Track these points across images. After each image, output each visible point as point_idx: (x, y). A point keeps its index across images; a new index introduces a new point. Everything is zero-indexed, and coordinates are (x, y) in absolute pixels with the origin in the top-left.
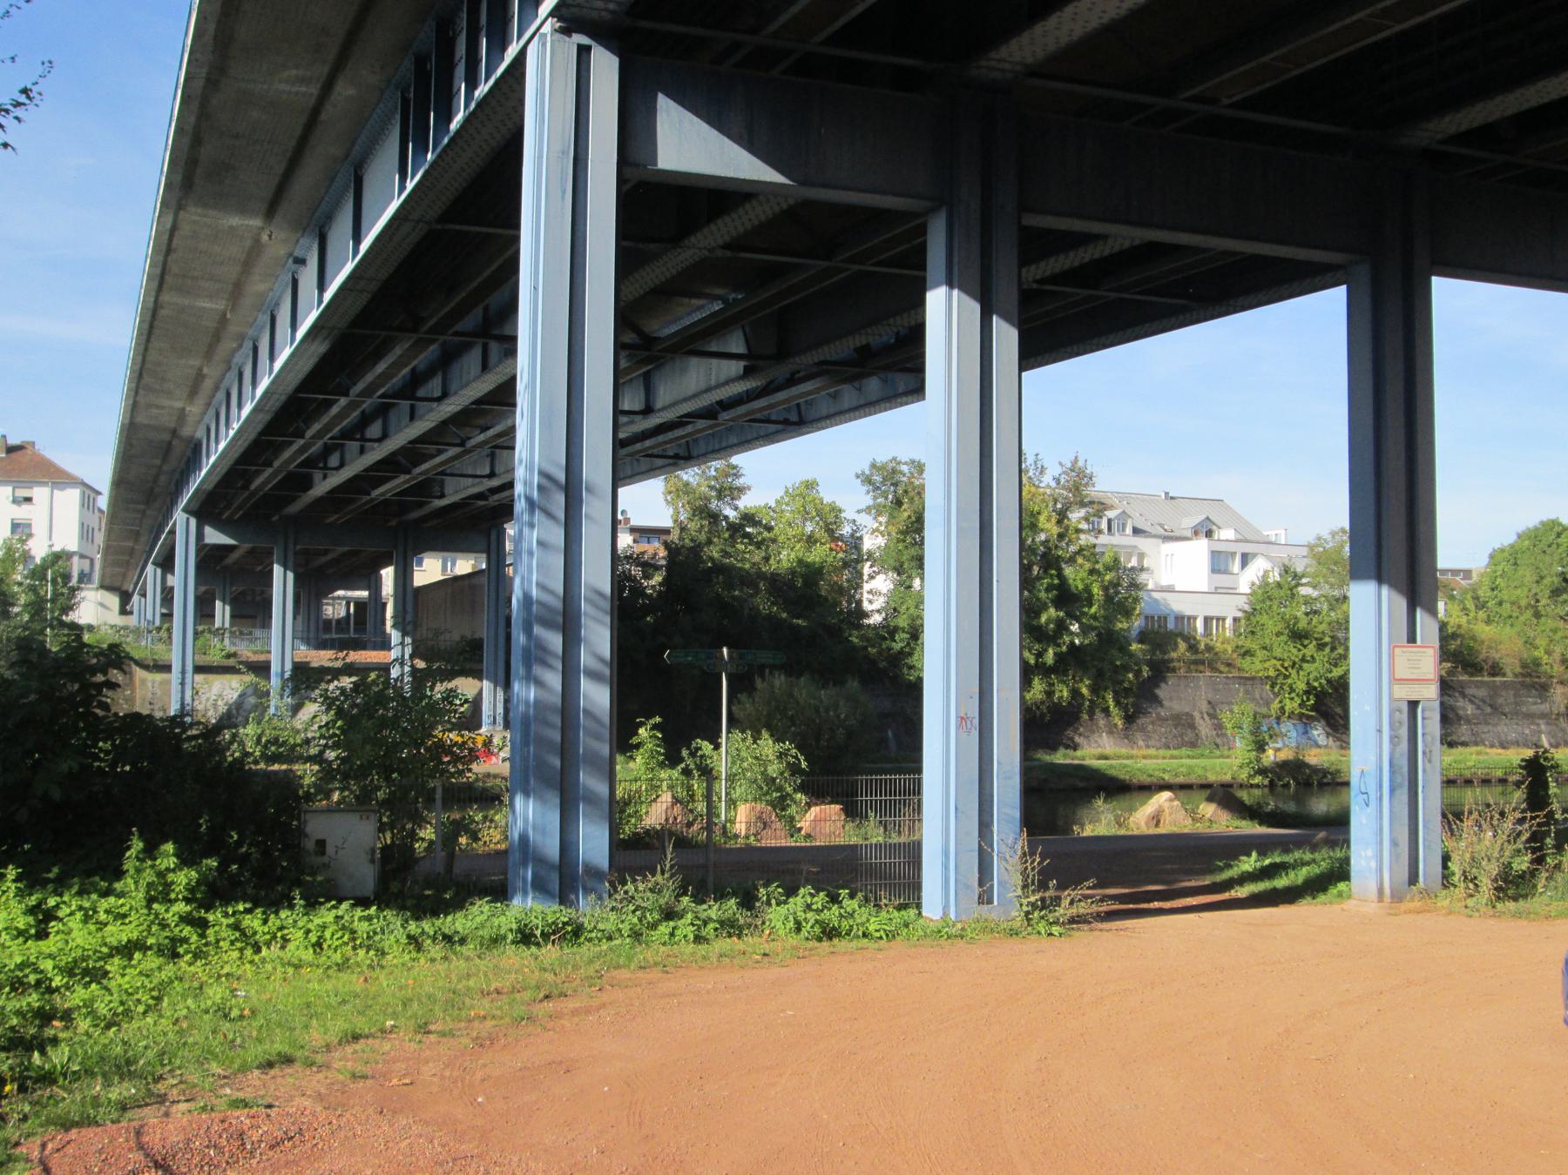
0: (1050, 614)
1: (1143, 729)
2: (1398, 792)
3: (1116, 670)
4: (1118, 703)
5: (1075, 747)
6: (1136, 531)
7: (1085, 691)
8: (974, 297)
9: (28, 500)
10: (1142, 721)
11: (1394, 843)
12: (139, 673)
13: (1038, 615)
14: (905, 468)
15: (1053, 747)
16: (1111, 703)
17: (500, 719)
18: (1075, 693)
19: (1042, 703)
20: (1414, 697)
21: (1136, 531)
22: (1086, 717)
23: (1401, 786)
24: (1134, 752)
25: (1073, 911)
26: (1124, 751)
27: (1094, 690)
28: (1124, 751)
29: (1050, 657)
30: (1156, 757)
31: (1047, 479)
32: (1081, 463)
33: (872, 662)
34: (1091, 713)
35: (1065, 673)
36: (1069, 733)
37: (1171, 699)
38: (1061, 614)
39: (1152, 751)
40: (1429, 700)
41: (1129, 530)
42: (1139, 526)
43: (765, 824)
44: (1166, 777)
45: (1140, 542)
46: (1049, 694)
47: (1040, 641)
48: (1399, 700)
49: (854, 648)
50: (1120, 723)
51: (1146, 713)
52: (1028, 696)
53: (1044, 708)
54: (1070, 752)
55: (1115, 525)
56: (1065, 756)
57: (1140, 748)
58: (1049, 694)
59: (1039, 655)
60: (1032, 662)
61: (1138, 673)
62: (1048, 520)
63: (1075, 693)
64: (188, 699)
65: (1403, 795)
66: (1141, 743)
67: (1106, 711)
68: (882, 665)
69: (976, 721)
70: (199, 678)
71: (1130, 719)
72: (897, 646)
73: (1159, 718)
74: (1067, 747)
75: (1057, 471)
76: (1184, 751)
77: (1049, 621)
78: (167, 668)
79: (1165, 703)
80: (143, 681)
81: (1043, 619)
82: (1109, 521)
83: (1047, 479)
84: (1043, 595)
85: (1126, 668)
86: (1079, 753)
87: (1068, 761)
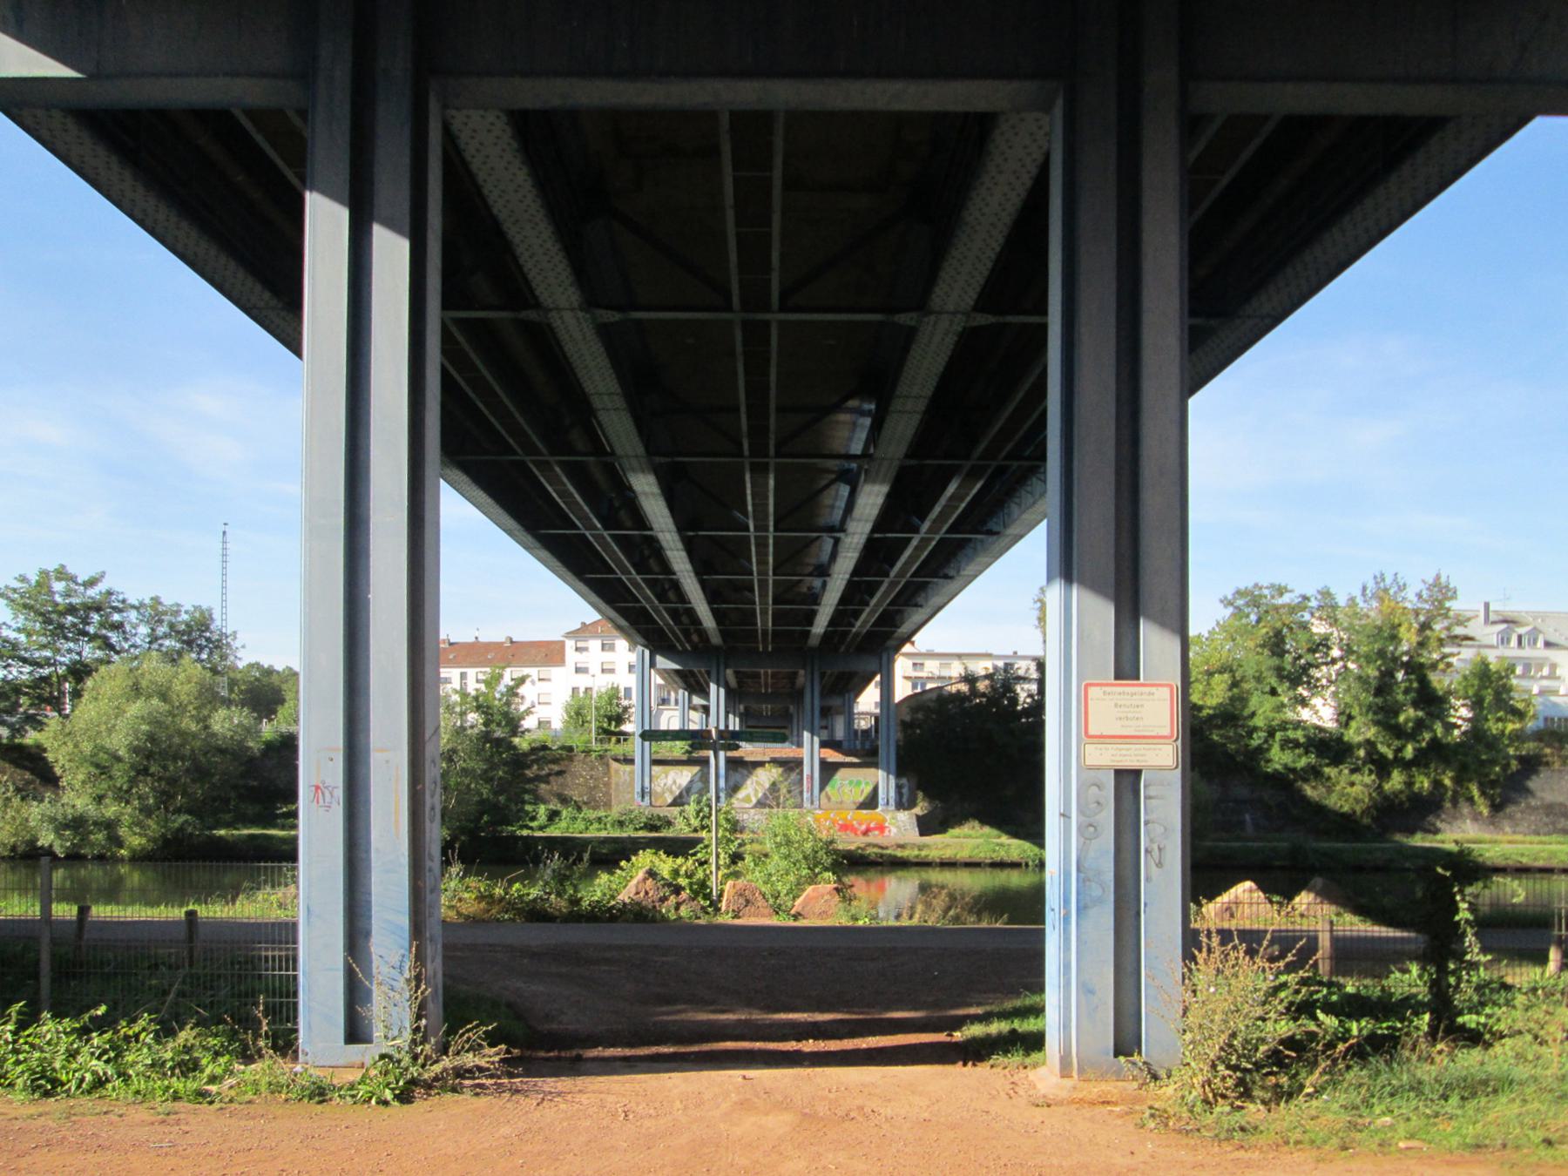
0: (1408, 715)
1: (1511, 817)
2: (1093, 912)
3: (1482, 763)
4: (1483, 793)
5: (1436, 831)
6: (1548, 644)
7: (1447, 782)
8: (341, 202)
9: (586, 649)
10: (1510, 809)
11: (1086, 990)
12: (614, 765)
13: (1397, 714)
14: (1266, 592)
15: (1411, 831)
16: (1476, 793)
17: (892, 802)
18: (1437, 784)
19: (1401, 792)
20: (1129, 763)
21: (1548, 644)
22: (1448, 805)
23: (1099, 901)
24: (1499, 837)
25: (458, 1061)
26: (1487, 836)
27: (1458, 781)
28: (1487, 836)
29: (1409, 751)
30: (1523, 842)
31: (1410, 594)
32: (1443, 580)
33: (1231, 757)
34: (1455, 802)
35: (1427, 766)
36: (1431, 818)
37: (1543, 790)
38: (1420, 714)
39: (1519, 837)
40: (1161, 769)
41: (1540, 644)
42: (1552, 639)
43: (748, 901)
44: (1524, 860)
45: (1552, 654)
46: (1409, 784)
47: (1398, 737)
48: (1099, 768)
49: (1214, 745)
50: (1485, 812)
51: (1515, 802)
52: (1387, 787)
53: (1403, 797)
54: (1430, 836)
55: (1525, 641)
56: (1423, 839)
57: (1505, 833)
58: (1409, 784)
59: (1399, 750)
60: (1390, 756)
61: (1506, 767)
62: (1409, 630)
63: (1437, 784)
64: (647, 784)
65: (1105, 917)
66: (1508, 829)
67: (1471, 800)
68: (1240, 758)
69: (340, 793)
70: (656, 769)
71: (1497, 808)
72: (1255, 742)
73: (1529, 806)
74: (1429, 831)
75: (1419, 587)
76: (1554, 838)
77: (1407, 720)
78: (631, 761)
79: (1539, 794)
80: (617, 771)
81: (1402, 718)
82: (1520, 638)
83: (1410, 594)
84: (1400, 697)
85: (1493, 762)
86: (1439, 837)
87: (1427, 845)
